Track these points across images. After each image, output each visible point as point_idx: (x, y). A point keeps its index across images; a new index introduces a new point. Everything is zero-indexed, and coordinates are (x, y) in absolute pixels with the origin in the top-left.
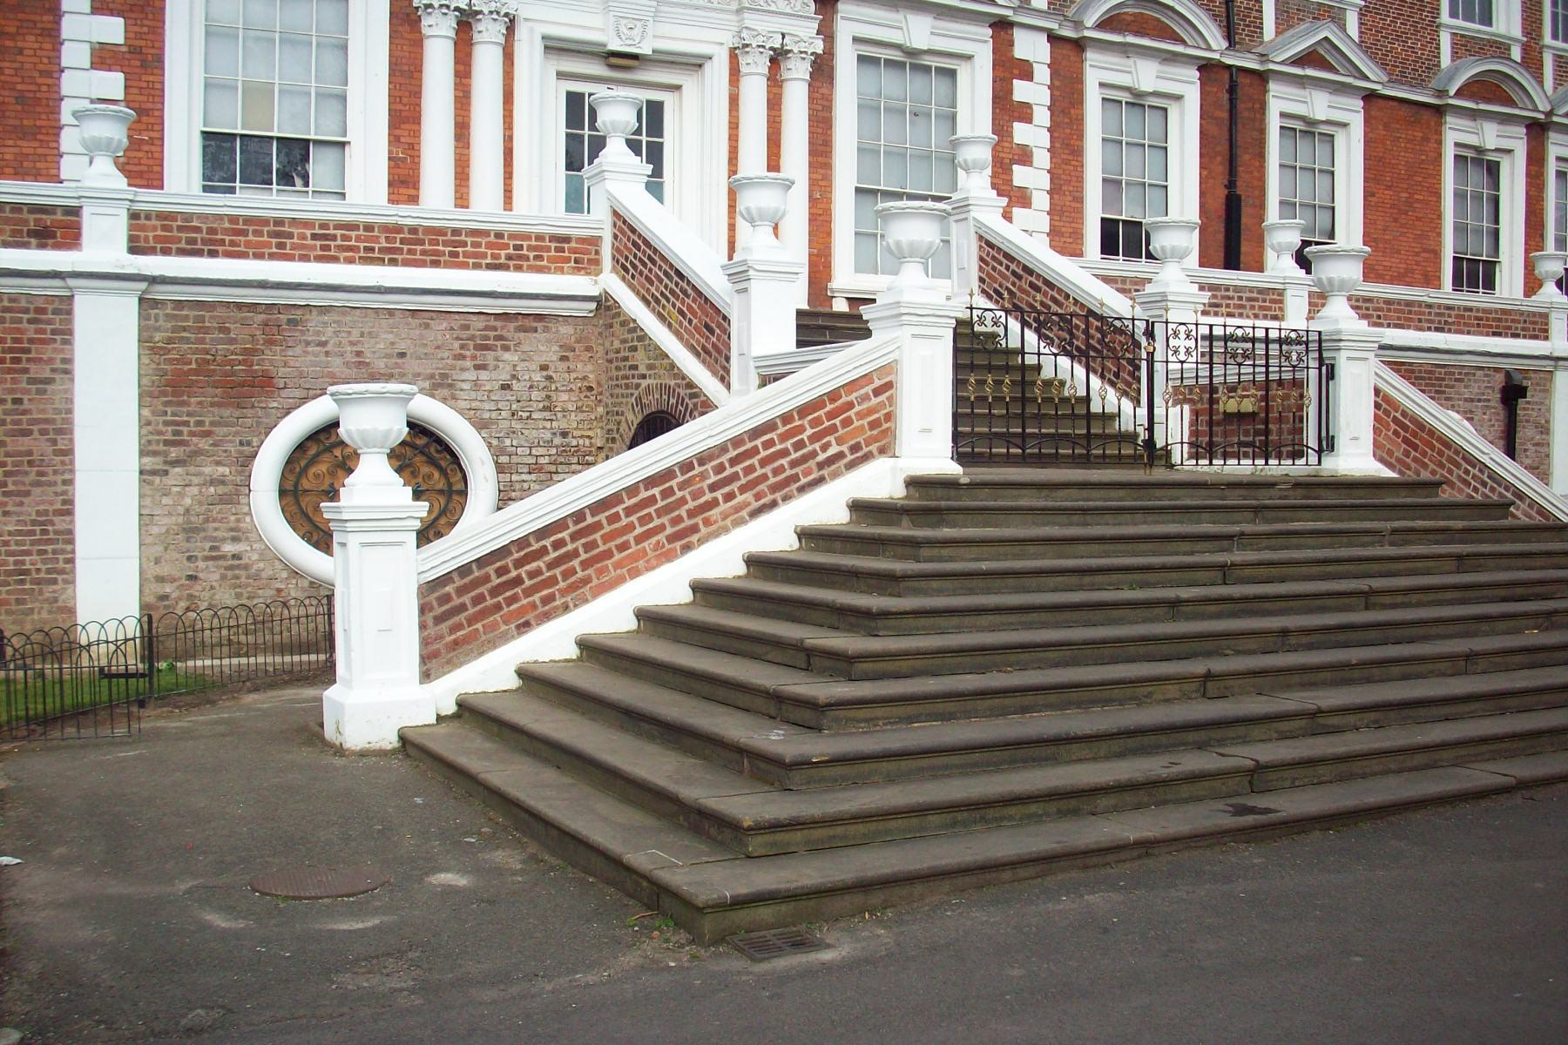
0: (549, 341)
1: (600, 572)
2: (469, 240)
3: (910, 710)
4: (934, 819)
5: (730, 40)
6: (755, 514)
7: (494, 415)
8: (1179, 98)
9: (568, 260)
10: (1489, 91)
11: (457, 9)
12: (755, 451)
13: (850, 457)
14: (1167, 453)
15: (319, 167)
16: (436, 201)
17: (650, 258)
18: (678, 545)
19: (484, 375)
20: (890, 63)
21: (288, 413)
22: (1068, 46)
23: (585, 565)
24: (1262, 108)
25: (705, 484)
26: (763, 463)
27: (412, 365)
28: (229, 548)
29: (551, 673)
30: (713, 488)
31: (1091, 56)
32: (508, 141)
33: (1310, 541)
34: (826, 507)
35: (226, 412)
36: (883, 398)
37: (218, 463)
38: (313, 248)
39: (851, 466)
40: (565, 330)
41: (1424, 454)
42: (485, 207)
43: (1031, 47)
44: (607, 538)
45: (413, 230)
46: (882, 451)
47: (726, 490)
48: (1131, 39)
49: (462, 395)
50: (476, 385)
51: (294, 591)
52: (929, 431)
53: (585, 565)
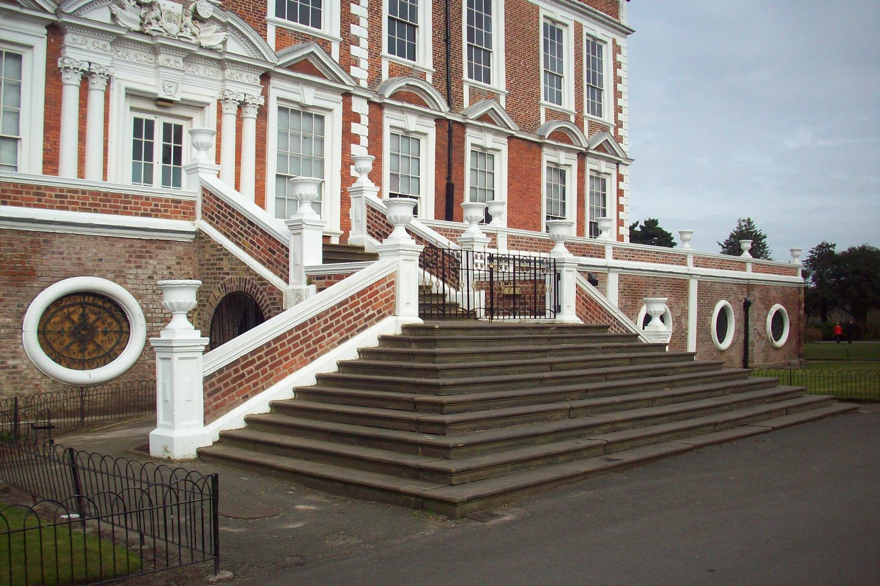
0: (171, 254)
2: (133, 201)
3: (472, 425)
4: (509, 467)
5: (217, 95)
6: (340, 342)
7: (145, 292)
8: (425, 134)
9: (180, 212)
10: (561, 136)
11: (82, 70)
14: (475, 313)
16: (67, 175)
17: (229, 213)
18: (309, 357)
19: (140, 271)
20: (293, 111)
21: (43, 290)
23: (271, 367)
24: (463, 141)
25: (320, 329)
27: (105, 265)
28: (11, 362)
29: (261, 417)
30: (323, 330)
31: (387, 112)
32: (106, 142)
33: (573, 352)
34: (369, 338)
35: (11, 289)
36: (390, 288)
37: (6, 316)
38: (56, 202)
39: (378, 320)
40: (180, 248)
41: (593, 313)
42: (93, 179)
43: (360, 107)
44: (280, 354)
45: (106, 194)
46: (390, 313)
47: (328, 331)
48: (406, 105)
49: (130, 281)
50: (137, 276)
51: (45, 387)
53: (271, 367)
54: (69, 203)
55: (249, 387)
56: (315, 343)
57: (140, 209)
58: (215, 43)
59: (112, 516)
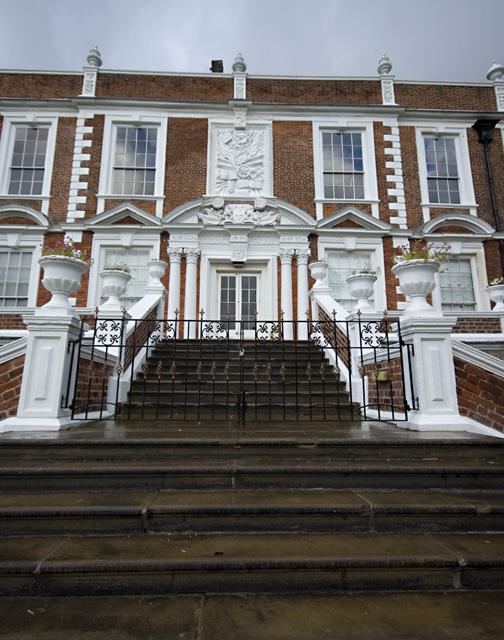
52: (441, 400)
59: (364, 407)
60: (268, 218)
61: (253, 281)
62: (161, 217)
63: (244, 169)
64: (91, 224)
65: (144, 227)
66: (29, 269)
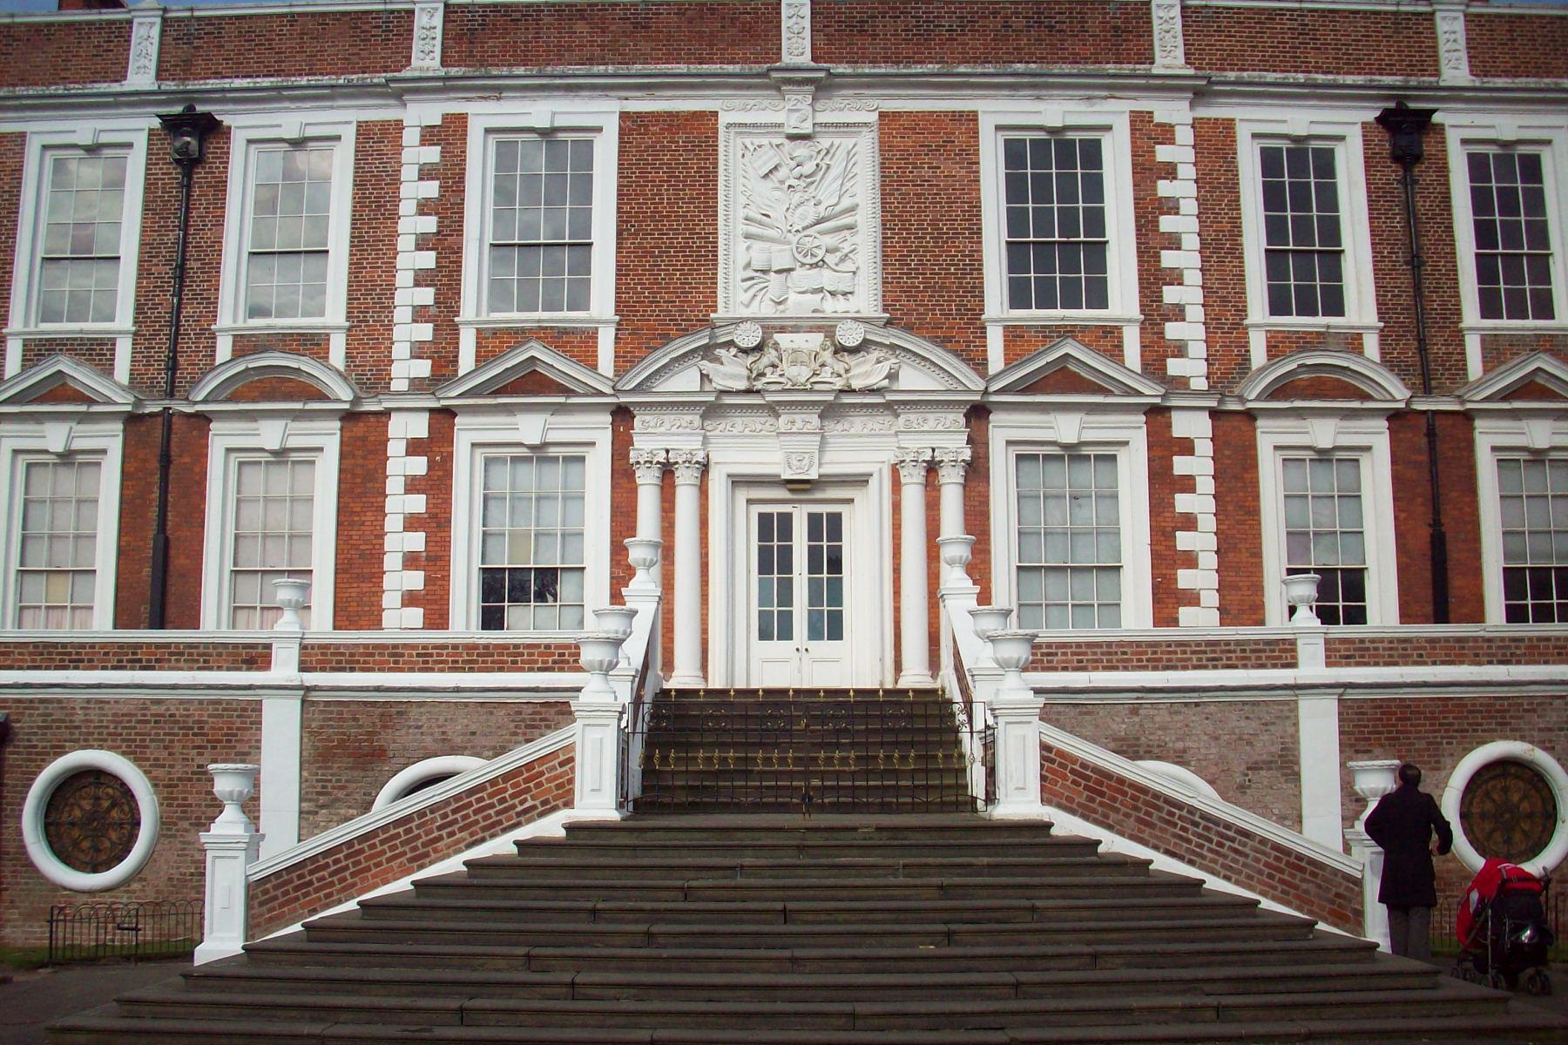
1: (362, 881)
12: (470, 804)
13: (541, 809)
15: (565, 587)
22: (1238, 418)
23: (353, 875)
26: (476, 812)
27: (480, 741)
30: (440, 828)
39: (542, 815)
53: (353, 875)
54: (435, 662)
55: (319, 899)
56: (424, 845)
57: (536, 662)
58: (876, 378)
60: (867, 372)
61: (835, 521)
62: (611, 374)
63: (808, 243)
64: (450, 396)
65: (95, 409)
66: (310, 500)
